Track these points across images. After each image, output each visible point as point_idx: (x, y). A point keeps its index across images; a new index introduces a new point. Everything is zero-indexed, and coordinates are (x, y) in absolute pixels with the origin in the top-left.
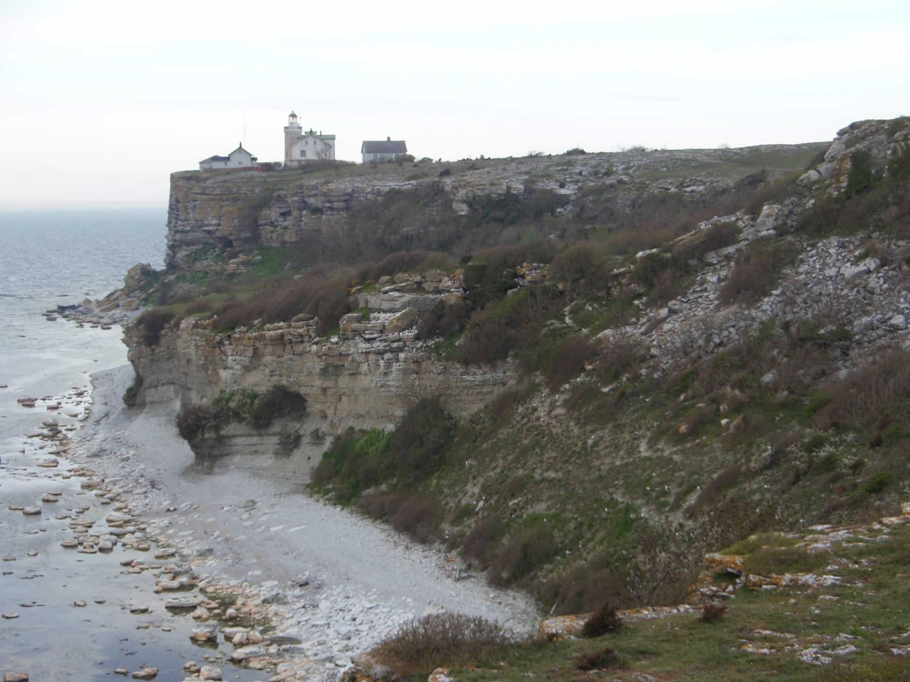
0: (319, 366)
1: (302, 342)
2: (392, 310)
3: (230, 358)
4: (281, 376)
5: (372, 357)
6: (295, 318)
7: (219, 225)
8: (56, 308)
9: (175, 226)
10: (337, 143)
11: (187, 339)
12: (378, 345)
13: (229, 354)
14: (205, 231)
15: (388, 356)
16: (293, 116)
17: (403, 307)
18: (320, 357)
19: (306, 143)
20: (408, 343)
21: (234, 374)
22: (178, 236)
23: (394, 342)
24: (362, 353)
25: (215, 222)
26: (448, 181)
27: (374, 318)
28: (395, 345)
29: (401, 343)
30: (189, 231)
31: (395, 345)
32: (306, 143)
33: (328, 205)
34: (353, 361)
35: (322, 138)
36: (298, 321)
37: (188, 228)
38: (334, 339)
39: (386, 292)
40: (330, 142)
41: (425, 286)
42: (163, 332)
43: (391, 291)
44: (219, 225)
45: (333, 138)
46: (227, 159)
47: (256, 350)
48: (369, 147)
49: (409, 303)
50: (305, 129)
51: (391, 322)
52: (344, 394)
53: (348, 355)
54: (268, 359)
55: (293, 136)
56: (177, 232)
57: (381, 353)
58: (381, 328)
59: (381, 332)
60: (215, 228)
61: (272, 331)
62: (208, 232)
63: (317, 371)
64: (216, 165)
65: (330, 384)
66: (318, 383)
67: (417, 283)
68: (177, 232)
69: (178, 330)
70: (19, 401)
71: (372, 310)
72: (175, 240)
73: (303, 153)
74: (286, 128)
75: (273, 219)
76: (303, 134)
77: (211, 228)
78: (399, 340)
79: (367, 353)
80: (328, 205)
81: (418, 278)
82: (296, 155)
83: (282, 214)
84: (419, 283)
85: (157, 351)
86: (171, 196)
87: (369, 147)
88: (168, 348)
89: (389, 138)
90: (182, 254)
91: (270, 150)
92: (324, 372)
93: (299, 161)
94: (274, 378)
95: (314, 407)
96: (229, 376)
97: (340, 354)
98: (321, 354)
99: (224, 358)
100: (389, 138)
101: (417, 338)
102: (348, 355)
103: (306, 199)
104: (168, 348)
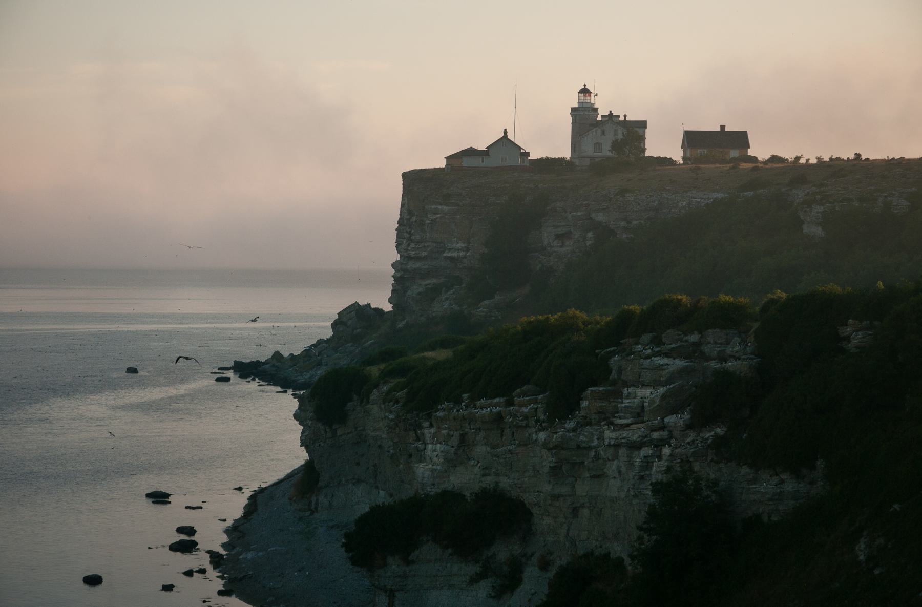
0: (547, 460)
1: (527, 426)
2: (655, 384)
3: (430, 446)
4: (497, 475)
5: (622, 452)
6: (518, 390)
7: (467, 250)
8: (231, 364)
9: (406, 250)
10: (649, 133)
11: (376, 417)
12: (635, 433)
13: (428, 440)
14: (447, 258)
15: (646, 451)
16: (585, 91)
17: (669, 381)
18: (549, 449)
19: (603, 133)
20: (676, 433)
21: (433, 471)
22: (411, 265)
23: (655, 430)
24: (609, 445)
25: (461, 245)
26: (799, 194)
27: (628, 397)
28: (656, 435)
29: (665, 434)
30: (425, 258)
31: (656, 435)
32: (603, 133)
33: (623, 224)
34: (597, 457)
35: (626, 124)
36: (525, 394)
37: (424, 254)
38: (571, 424)
39: (648, 357)
40: (640, 131)
41: (706, 349)
42: (350, 405)
43: (656, 354)
44: (467, 250)
45: (643, 125)
46: (485, 153)
47: (463, 437)
48: (692, 139)
49: (681, 372)
50: (603, 111)
51: (652, 402)
52: (583, 506)
53: (590, 448)
54: (481, 450)
55: (584, 118)
56: (410, 258)
57: (635, 446)
58: (638, 411)
59: (639, 415)
60: (462, 254)
61: (488, 408)
62: (452, 259)
63: (546, 469)
64: (467, 162)
65: (564, 490)
66: (547, 488)
67: (694, 344)
68: (410, 258)
69: (368, 402)
70: (149, 496)
71: (626, 384)
72: (405, 271)
73: (598, 146)
74: (573, 109)
75: (546, 243)
76: (599, 118)
77: (455, 254)
78: (662, 428)
79: (617, 446)
80: (623, 224)
81: (694, 338)
82: (588, 148)
83: (558, 237)
84: (697, 345)
85: (339, 432)
86: (402, 206)
87: (692, 139)
88: (356, 428)
89: (723, 127)
90: (415, 289)
91: (548, 138)
92: (555, 471)
93: (592, 158)
94: (489, 478)
95: (543, 522)
96: (427, 473)
97: (579, 447)
98: (551, 445)
99: (421, 446)
100: (723, 127)
101: (689, 426)
102: (590, 448)
103: (593, 215)
104: (356, 428)
